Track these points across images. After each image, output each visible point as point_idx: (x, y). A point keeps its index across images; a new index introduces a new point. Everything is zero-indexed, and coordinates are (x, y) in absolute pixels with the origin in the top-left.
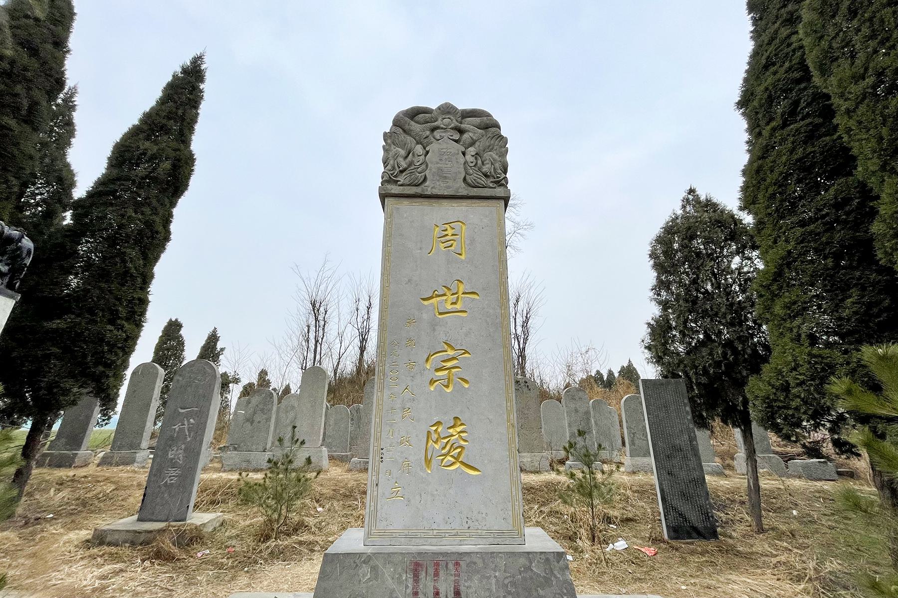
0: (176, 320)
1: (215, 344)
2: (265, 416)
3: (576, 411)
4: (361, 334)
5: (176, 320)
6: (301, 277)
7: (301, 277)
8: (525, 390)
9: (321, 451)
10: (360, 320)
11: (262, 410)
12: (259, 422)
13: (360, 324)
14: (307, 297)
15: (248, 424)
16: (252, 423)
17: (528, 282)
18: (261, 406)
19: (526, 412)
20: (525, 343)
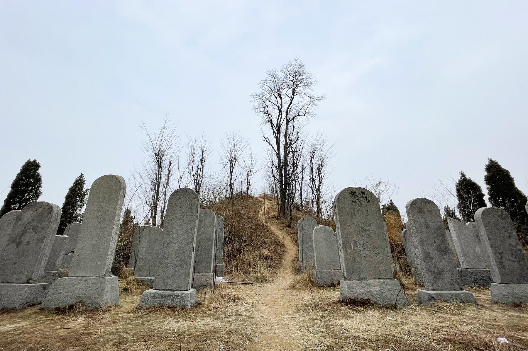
0: (35, 161)
1: (82, 187)
2: (37, 236)
3: (427, 226)
4: (195, 179)
5: (35, 161)
6: (147, 134)
7: (147, 134)
8: (363, 201)
9: (103, 282)
10: (195, 168)
11: (35, 229)
12: (28, 243)
13: (194, 173)
14: (151, 148)
15: (14, 245)
16: (19, 244)
17: (320, 141)
18: (34, 224)
19: (367, 228)
20: (320, 186)
